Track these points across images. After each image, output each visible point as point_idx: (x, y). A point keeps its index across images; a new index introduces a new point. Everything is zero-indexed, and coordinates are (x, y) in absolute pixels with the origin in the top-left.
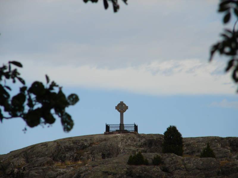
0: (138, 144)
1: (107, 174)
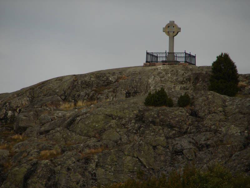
0: (179, 79)
1: (111, 118)
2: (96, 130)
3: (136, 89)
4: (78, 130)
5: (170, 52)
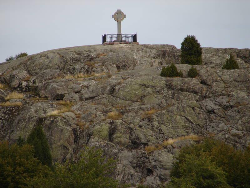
1: (144, 86)
2: (137, 96)
3: (124, 64)
4: (122, 96)
5: (119, 34)
